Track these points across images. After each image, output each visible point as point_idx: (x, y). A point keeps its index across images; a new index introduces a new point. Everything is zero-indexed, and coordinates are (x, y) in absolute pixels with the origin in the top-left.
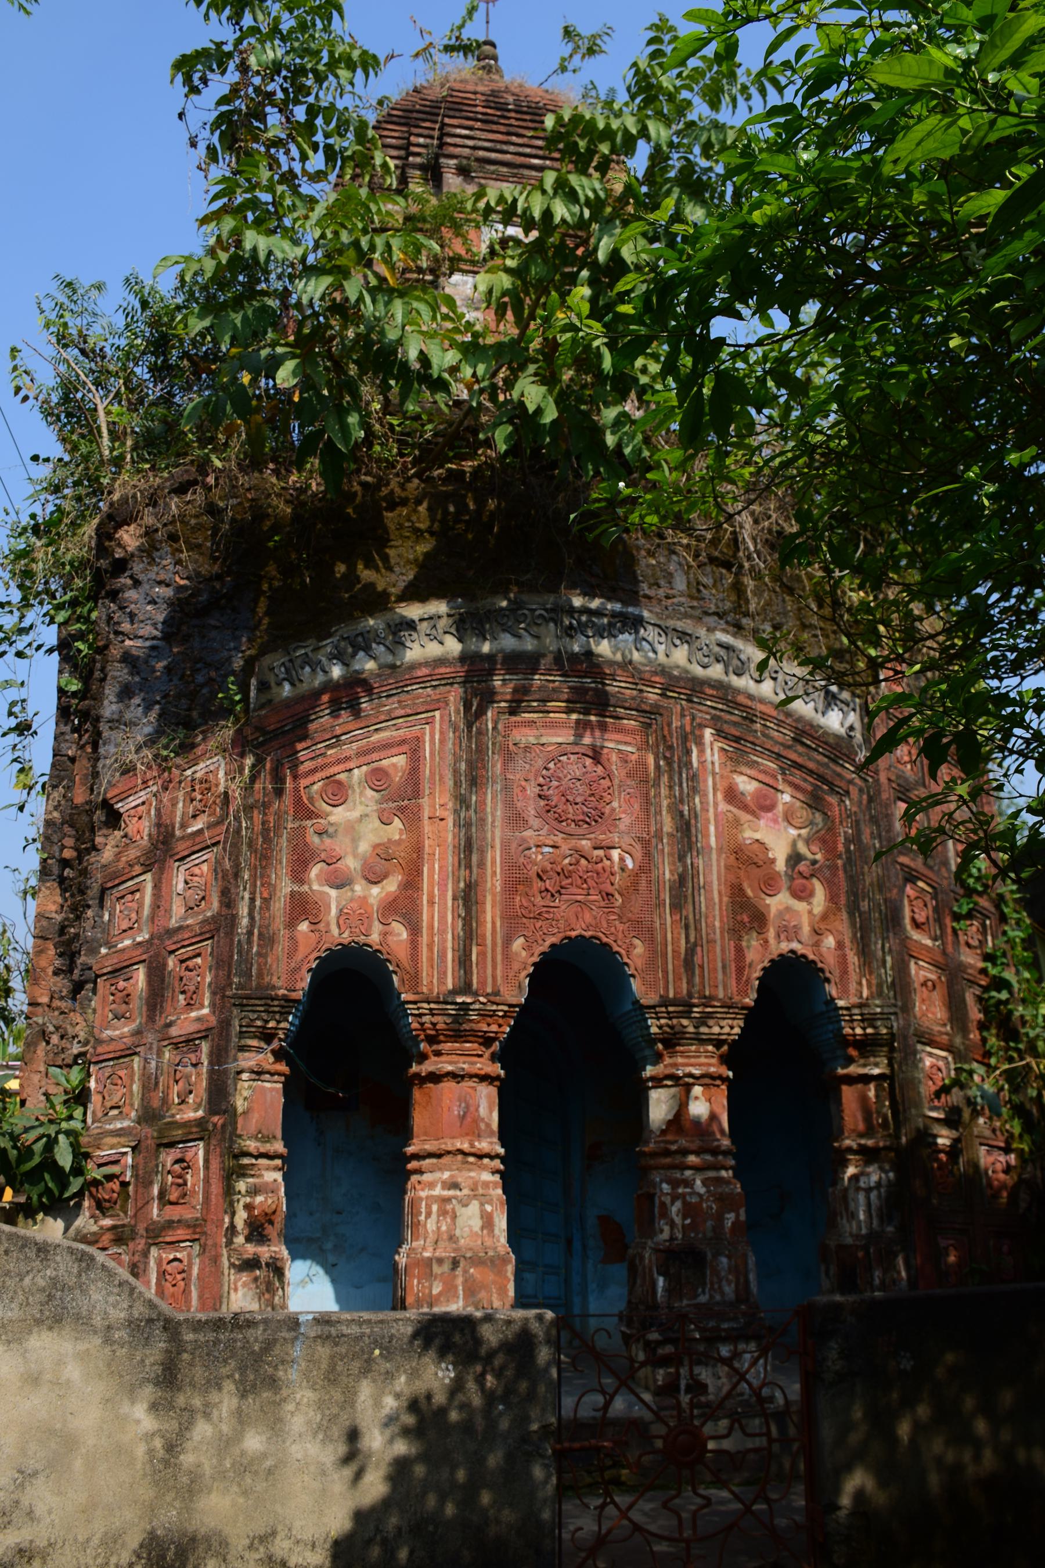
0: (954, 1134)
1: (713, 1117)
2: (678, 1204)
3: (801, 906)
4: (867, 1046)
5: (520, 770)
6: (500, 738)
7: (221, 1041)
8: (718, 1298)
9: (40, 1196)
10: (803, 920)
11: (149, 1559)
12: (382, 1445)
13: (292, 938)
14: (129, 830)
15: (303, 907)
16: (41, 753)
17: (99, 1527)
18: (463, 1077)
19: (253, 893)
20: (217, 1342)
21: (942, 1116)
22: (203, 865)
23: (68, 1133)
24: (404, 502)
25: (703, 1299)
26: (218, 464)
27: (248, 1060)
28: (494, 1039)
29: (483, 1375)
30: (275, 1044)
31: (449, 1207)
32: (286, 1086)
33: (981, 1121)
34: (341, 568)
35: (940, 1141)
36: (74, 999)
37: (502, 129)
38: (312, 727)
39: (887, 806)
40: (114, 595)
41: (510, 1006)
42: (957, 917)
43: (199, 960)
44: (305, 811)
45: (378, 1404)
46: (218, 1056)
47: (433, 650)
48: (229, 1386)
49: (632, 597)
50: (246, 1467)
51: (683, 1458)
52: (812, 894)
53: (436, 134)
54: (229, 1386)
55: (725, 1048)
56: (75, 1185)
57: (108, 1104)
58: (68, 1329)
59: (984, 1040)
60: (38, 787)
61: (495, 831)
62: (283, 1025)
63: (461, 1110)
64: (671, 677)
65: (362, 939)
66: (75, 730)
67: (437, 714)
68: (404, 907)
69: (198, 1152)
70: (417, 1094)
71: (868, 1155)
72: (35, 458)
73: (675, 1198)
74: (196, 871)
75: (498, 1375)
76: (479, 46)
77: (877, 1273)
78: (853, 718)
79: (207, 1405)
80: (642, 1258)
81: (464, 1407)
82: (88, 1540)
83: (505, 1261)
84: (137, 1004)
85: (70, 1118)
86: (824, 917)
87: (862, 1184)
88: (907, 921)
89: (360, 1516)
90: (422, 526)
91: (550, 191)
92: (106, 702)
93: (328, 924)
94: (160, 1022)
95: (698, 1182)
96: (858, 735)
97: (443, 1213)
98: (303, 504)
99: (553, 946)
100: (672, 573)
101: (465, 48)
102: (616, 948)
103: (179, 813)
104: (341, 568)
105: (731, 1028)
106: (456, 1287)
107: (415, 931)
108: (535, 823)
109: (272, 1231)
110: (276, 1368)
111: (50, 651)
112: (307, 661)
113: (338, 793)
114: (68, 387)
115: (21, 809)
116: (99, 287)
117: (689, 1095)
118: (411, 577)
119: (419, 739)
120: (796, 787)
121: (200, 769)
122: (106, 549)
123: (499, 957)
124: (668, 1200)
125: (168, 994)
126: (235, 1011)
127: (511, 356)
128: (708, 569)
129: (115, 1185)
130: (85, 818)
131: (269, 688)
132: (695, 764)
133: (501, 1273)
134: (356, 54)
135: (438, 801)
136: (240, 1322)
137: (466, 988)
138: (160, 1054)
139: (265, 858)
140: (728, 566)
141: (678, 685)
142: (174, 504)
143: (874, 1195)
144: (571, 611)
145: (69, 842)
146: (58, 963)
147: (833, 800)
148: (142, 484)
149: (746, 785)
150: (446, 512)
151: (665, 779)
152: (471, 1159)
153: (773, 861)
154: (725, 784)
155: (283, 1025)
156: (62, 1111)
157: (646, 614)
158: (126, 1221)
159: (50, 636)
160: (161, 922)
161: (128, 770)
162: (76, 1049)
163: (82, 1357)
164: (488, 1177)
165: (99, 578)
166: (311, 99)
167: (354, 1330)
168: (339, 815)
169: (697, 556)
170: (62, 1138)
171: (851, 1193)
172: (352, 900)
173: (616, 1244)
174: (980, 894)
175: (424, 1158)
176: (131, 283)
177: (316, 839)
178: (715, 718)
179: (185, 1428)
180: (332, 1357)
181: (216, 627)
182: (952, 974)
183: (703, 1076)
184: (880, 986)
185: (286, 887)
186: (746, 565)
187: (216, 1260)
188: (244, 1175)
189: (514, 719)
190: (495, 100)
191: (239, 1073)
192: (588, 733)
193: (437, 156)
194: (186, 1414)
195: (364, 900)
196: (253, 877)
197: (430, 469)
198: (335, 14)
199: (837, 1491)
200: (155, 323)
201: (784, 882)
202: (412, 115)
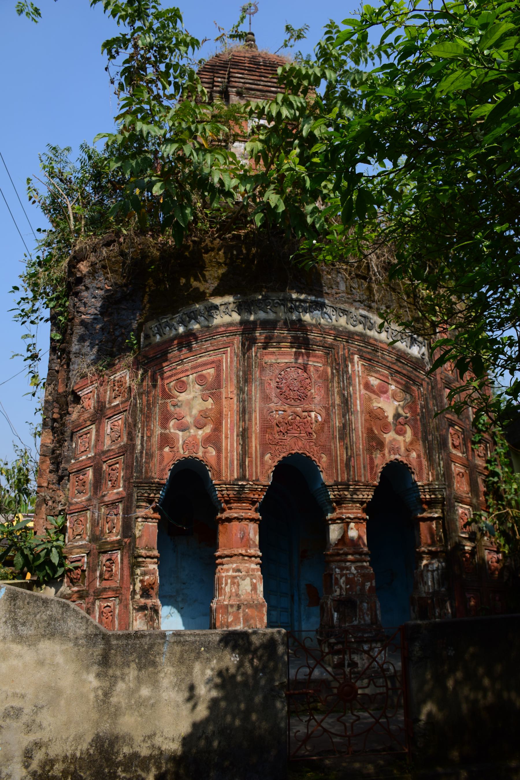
1: (360, 537)
2: (344, 578)
3: (400, 438)
4: (431, 504)
7: (128, 503)
8: (362, 622)
9: (44, 577)
10: (401, 445)
13: (161, 455)
15: (166, 440)
17: (73, 732)
18: (242, 519)
22: (119, 421)
23: (57, 547)
24: (212, 249)
25: (355, 623)
26: (125, 232)
27: (141, 512)
28: (256, 502)
29: (252, 659)
30: (154, 505)
31: (236, 581)
33: (486, 538)
34: (183, 281)
35: (466, 548)
36: (59, 484)
37: (257, 74)
39: (440, 391)
40: (76, 294)
42: (474, 443)
43: (117, 465)
45: (203, 673)
46: (127, 510)
47: (227, 319)
48: (133, 665)
50: (142, 703)
51: (347, 698)
52: (405, 432)
53: (226, 76)
54: (133, 665)
57: (76, 533)
59: (487, 501)
60: (41, 385)
61: (257, 404)
63: (241, 536)
64: (338, 331)
65: (194, 455)
66: (58, 358)
67: (229, 349)
68: (214, 440)
70: (220, 528)
71: (433, 555)
72: (39, 230)
75: (260, 659)
76: (246, 35)
77: (437, 610)
78: (424, 350)
79: (123, 674)
80: (327, 604)
81: (244, 674)
82: (67, 738)
83: (262, 606)
84: (88, 486)
85: (58, 540)
86: (411, 443)
89: (195, 726)
91: (280, 103)
93: (178, 448)
94: (100, 495)
95: (353, 568)
96: (426, 358)
97: (233, 583)
98: (165, 251)
99: (284, 457)
100: (339, 282)
101: (240, 36)
102: (313, 459)
103: (108, 397)
104: (183, 281)
105: (368, 495)
107: (219, 451)
108: (275, 400)
109: (153, 593)
110: (155, 657)
111: (47, 321)
112: (167, 324)
113: (182, 387)
114: (54, 197)
115: (34, 395)
116: (68, 149)
120: (398, 382)
121: (118, 376)
122: (72, 273)
123: (259, 463)
124: (339, 577)
126: (135, 489)
127: (262, 181)
128: (356, 280)
129: (79, 571)
132: (350, 372)
133: (260, 611)
135: (229, 390)
136: (138, 635)
137: (243, 477)
138: (99, 510)
139: (148, 417)
140: (365, 278)
143: (435, 573)
144: (292, 300)
145: (56, 410)
147: (415, 388)
148: (89, 242)
149: (374, 381)
150: (232, 254)
151: (336, 379)
152: (246, 558)
154: (364, 381)
157: (326, 301)
159: (46, 313)
161: (84, 376)
162: (60, 508)
164: (254, 566)
165: (69, 286)
166: (167, 61)
167: (192, 639)
168: (183, 397)
169: (350, 274)
172: (189, 437)
173: (314, 597)
174: (484, 432)
175: (224, 557)
177: (172, 408)
179: (113, 685)
180: (181, 651)
181: (124, 309)
182: (471, 470)
184: (437, 475)
186: (374, 278)
187: (126, 606)
188: (140, 566)
190: (254, 60)
191: (137, 518)
192: (301, 358)
193: (227, 87)
194: (113, 678)
195: (195, 436)
196: (143, 427)
197: (224, 234)
198: (178, 20)
199: (419, 712)
201: (392, 427)
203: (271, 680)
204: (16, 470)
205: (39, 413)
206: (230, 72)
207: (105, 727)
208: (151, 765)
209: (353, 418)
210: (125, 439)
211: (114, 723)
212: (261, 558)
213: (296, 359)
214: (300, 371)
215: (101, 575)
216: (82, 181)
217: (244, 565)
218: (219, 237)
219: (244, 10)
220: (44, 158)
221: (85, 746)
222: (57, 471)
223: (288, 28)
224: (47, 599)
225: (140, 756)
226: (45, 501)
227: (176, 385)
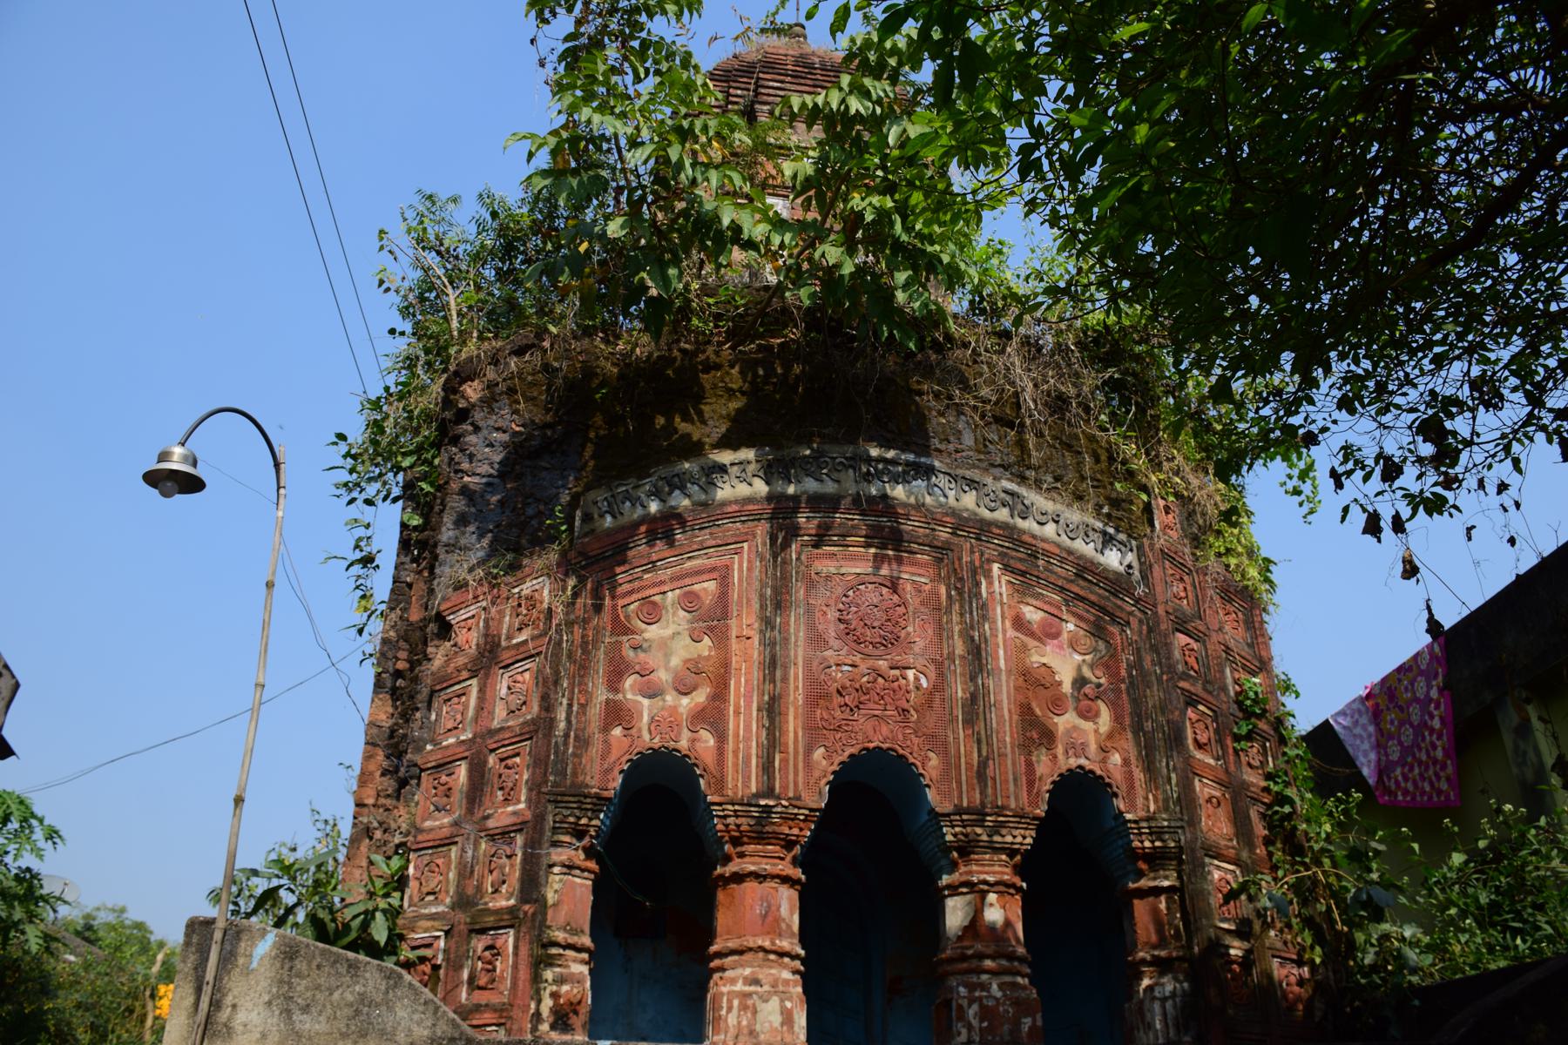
0: (1246, 945)
1: (1008, 923)
2: (975, 1007)
4: (1156, 859)
5: (820, 597)
7: (533, 830)
10: (1089, 738)
15: (617, 714)
16: (381, 583)
19: (571, 700)
22: (525, 675)
24: (718, 367)
27: (560, 855)
28: (796, 843)
30: (586, 841)
31: (750, 1002)
32: (597, 889)
35: (1232, 952)
38: (630, 554)
39: (1166, 636)
40: (455, 440)
41: (811, 810)
43: (518, 760)
44: (621, 628)
46: (532, 844)
47: (743, 490)
49: (925, 450)
52: (1097, 714)
57: (425, 890)
59: (1270, 854)
61: (798, 651)
62: (594, 822)
63: (763, 910)
64: (960, 517)
67: (745, 545)
68: (712, 717)
69: (509, 939)
73: (971, 1001)
74: (519, 678)
76: (791, 27)
78: (1131, 557)
84: (458, 798)
86: (1110, 736)
88: (1190, 741)
91: (847, 89)
93: (640, 730)
94: (478, 815)
95: (995, 986)
98: (628, 365)
99: (851, 756)
101: (779, 31)
102: (911, 760)
105: (1023, 838)
107: (721, 738)
108: (836, 644)
112: (627, 497)
113: (653, 613)
114: (427, 285)
115: (360, 632)
117: (984, 903)
118: (724, 429)
119: (728, 568)
120: (1080, 618)
121: (526, 588)
123: (801, 765)
124: (965, 1003)
125: (487, 789)
126: (550, 807)
127: (812, 234)
129: (427, 968)
130: (418, 633)
131: (592, 518)
135: (745, 621)
139: (583, 668)
140: (1011, 425)
141: (963, 524)
142: (513, 363)
143: (1169, 1004)
144: (869, 460)
145: (403, 655)
146: (385, 764)
147: (1114, 629)
149: (1032, 614)
150: (755, 375)
152: (772, 957)
153: (1060, 684)
155: (594, 822)
157: (937, 464)
160: (484, 723)
161: (460, 586)
162: (397, 839)
164: (787, 975)
165: (443, 428)
166: (644, 35)
168: (652, 632)
169: (983, 417)
171: (1147, 1004)
175: (726, 955)
176: (484, 198)
177: (631, 653)
182: (1236, 794)
184: (1166, 800)
185: (601, 695)
186: (1028, 422)
188: (551, 965)
192: (886, 566)
195: (674, 709)
196: (572, 685)
200: (502, 231)
201: (1071, 703)
202: (725, 76)
205: (368, 663)
206: (758, 78)
212: (803, 961)
213: (877, 568)
214: (885, 590)
220: (410, 214)
227: (640, 608)
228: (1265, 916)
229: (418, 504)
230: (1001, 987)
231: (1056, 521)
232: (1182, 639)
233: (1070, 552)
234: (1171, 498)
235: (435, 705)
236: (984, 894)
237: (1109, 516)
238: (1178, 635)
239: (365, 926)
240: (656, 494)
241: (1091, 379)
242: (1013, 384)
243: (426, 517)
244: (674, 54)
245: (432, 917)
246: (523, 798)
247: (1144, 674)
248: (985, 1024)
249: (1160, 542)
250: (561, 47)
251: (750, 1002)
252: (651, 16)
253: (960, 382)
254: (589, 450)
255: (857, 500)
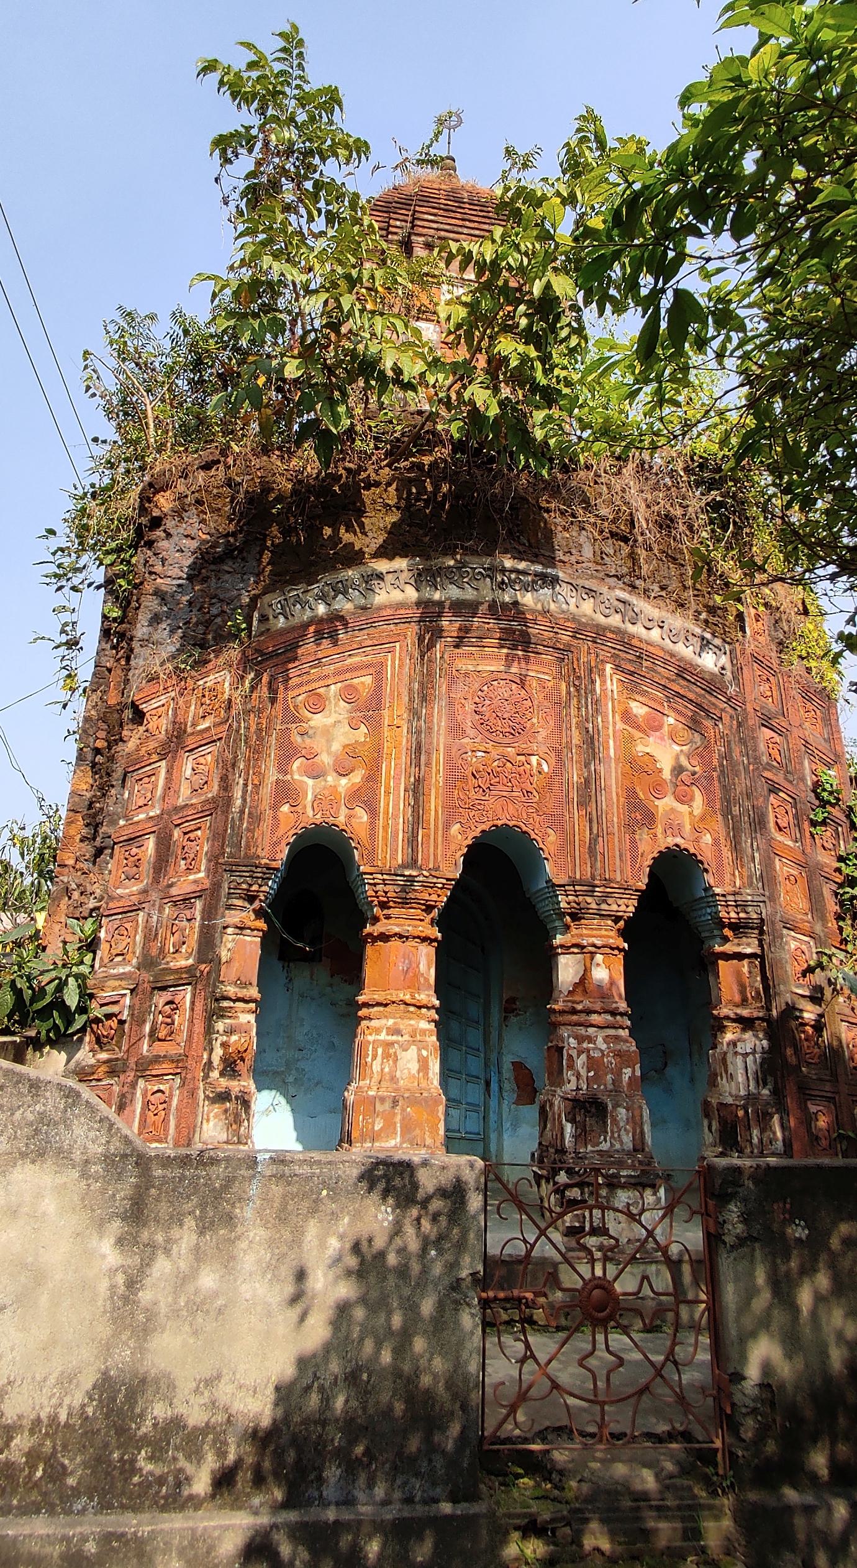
1: (612, 982)
2: (583, 1057)
3: (684, 809)
4: (739, 928)
6: (445, 665)
7: (212, 900)
8: (618, 1146)
9: (48, 1031)
10: (685, 821)
11: (100, 1401)
12: (329, 1287)
13: (275, 818)
14: (150, 726)
15: (286, 792)
17: (57, 1366)
18: (407, 938)
19: (246, 780)
20: (182, 1178)
21: (807, 993)
22: (208, 756)
23: (77, 977)
24: (377, 484)
25: (604, 1146)
26: (237, 449)
27: (233, 917)
28: (434, 907)
29: (418, 1220)
30: (256, 904)
31: (392, 1051)
32: (264, 945)
33: (841, 999)
34: (327, 531)
35: (806, 1015)
36: (94, 863)
37: (459, 216)
38: (300, 651)
39: (753, 730)
40: (150, 544)
41: (448, 880)
42: (814, 824)
43: (199, 833)
45: (323, 1245)
46: (209, 913)
47: (396, 596)
48: (190, 1223)
49: (551, 561)
50: (197, 1307)
51: (598, 1309)
52: (692, 799)
53: (409, 219)
54: (190, 1223)
55: (622, 923)
56: (80, 1021)
57: (114, 952)
58: (49, 1162)
59: (841, 929)
60: (81, 690)
61: (440, 739)
62: (263, 889)
63: (404, 965)
64: (579, 623)
65: (331, 820)
66: (113, 647)
67: (397, 644)
68: (366, 797)
69: (186, 995)
70: (369, 950)
71: (746, 1023)
72: (95, 440)
74: (202, 760)
75: (435, 1218)
76: (442, 159)
77: (755, 1132)
78: (724, 660)
79: (168, 1241)
80: (552, 1105)
81: (402, 1251)
82: (45, 1380)
83: (436, 1102)
84: (146, 868)
85: (82, 963)
86: (702, 819)
87: (739, 1049)
88: (772, 825)
89: (302, 1363)
90: (390, 502)
91: (499, 241)
92: (138, 626)
93: (305, 807)
94: (164, 882)
95: (600, 1039)
96: (728, 674)
97: (387, 1056)
98: (300, 482)
99: (483, 831)
100: (578, 542)
101: (432, 162)
102: (533, 836)
103: (191, 714)
104: (327, 531)
105: (628, 907)
106: (395, 1123)
107: (373, 812)
108: (471, 732)
109: (241, 1067)
110: (233, 1205)
111: (98, 587)
112: (297, 600)
113: (318, 704)
114: (126, 393)
115: (64, 707)
116: (152, 317)
117: (590, 963)
118: (381, 541)
120: (679, 713)
121: (210, 681)
122: (146, 509)
123: (440, 839)
124: (574, 1053)
125: (172, 860)
126: (226, 875)
127: (463, 373)
128: (610, 541)
129: (114, 1023)
130: (116, 716)
131: (268, 619)
132: (598, 692)
133: (433, 1112)
134: (351, 140)
135: (395, 713)
136: (205, 1160)
137: (413, 863)
138: (161, 910)
139: (257, 751)
140: (625, 540)
141: (582, 630)
143: (750, 1059)
144: (503, 571)
145: (102, 734)
146: (84, 831)
147: (708, 723)
148: (178, 462)
149: (638, 709)
150: (410, 493)
151: (574, 702)
152: (412, 1009)
153: (660, 771)
154: (622, 708)
155: (263, 889)
156: (75, 956)
157: (561, 574)
158: (120, 1055)
159: (98, 575)
160: (171, 802)
161: (153, 678)
162: (92, 904)
163: (60, 1190)
164: (425, 1024)
165: (139, 532)
166: (317, 176)
167: (305, 1170)
168: (317, 720)
169: (601, 532)
170: (71, 980)
172: (325, 788)
173: (527, 1088)
174: (833, 805)
175: (373, 1006)
176: (177, 316)
177: (299, 739)
178: (614, 656)
179: (146, 1264)
180: (284, 1196)
181: (229, 573)
182: (811, 871)
183: (604, 946)
184: (750, 877)
186: (640, 539)
187: (193, 1093)
188: (223, 1016)
189: (457, 651)
190: (454, 195)
191: (225, 928)
192: (516, 664)
193: (409, 237)
194: (149, 1249)
195: (335, 788)
196: (248, 767)
197: (398, 461)
198: (336, 107)
199: (743, 1358)
201: (670, 788)
203: (453, 1266)
204: (39, 840)
205: (72, 738)
206: (415, 211)
207: (123, 1355)
208: (206, 1447)
209: (602, 769)
210: (216, 787)
211: (142, 1350)
212: (438, 1011)
213: (509, 666)
214: (514, 686)
215: (153, 1031)
216: (172, 369)
217: (406, 1022)
218: (389, 465)
219: (440, 122)
220: (112, 328)
221: (77, 1398)
222: (94, 839)
223: (509, 152)
224: (38, 1080)
225: (185, 1427)
226: (68, 892)
227: (307, 700)
228: (835, 984)
229: (117, 598)
230: (607, 1039)
231: (664, 628)
232: (767, 733)
233: (672, 655)
234: (761, 608)
235: (128, 784)
236: (593, 954)
237: (706, 621)
238: (763, 729)
239: (60, 988)
240: (323, 597)
241: (697, 500)
242: (627, 504)
243: (124, 609)
244: (343, 195)
245: (120, 977)
246: (203, 868)
247: (733, 764)
248: (592, 1074)
249: (750, 648)
250: (242, 185)
251: (392, 1051)
252: (323, 160)
253: (584, 501)
254: (267, 556)
255: (493, 605)
